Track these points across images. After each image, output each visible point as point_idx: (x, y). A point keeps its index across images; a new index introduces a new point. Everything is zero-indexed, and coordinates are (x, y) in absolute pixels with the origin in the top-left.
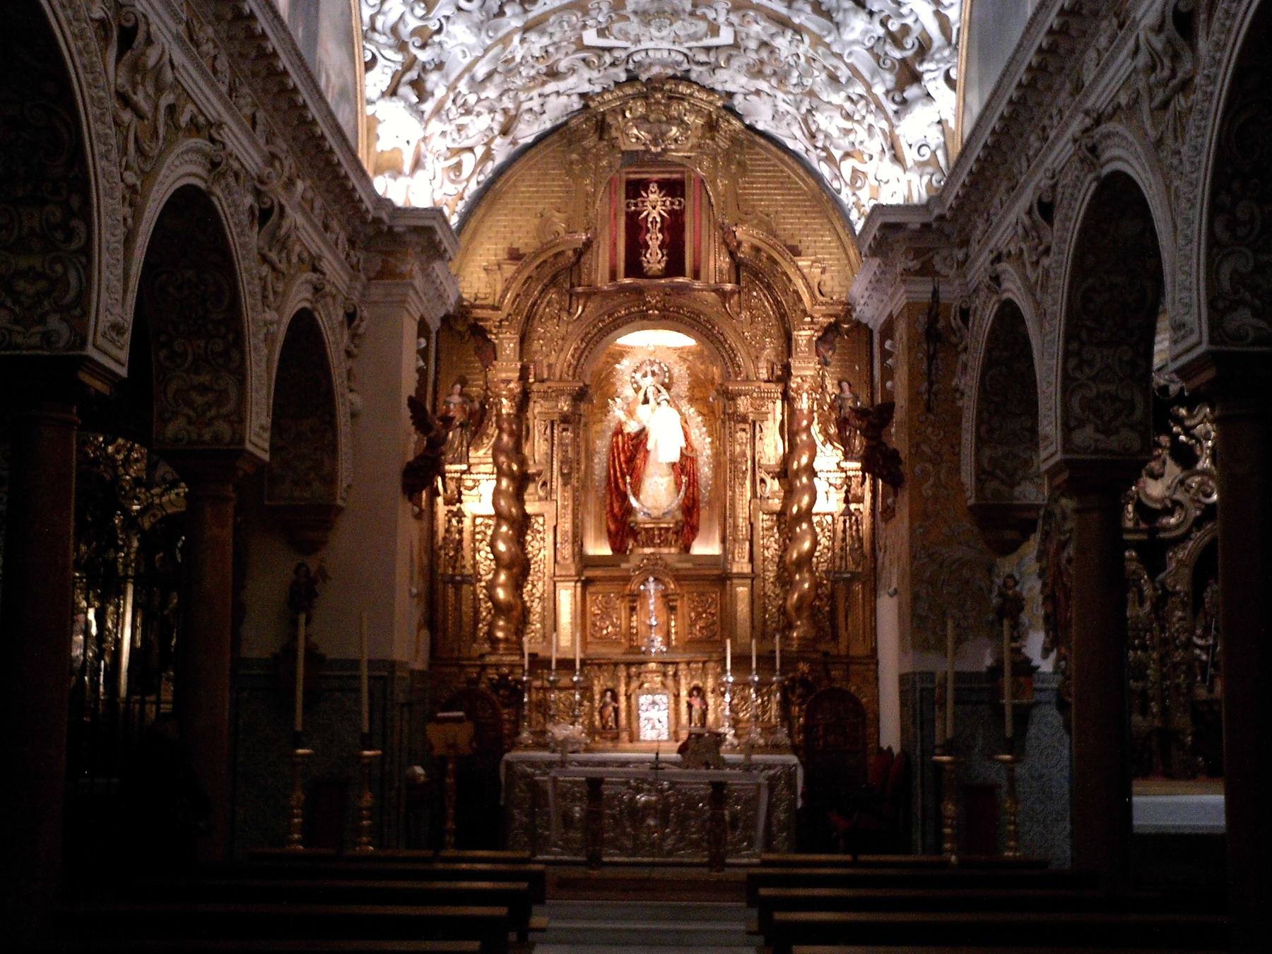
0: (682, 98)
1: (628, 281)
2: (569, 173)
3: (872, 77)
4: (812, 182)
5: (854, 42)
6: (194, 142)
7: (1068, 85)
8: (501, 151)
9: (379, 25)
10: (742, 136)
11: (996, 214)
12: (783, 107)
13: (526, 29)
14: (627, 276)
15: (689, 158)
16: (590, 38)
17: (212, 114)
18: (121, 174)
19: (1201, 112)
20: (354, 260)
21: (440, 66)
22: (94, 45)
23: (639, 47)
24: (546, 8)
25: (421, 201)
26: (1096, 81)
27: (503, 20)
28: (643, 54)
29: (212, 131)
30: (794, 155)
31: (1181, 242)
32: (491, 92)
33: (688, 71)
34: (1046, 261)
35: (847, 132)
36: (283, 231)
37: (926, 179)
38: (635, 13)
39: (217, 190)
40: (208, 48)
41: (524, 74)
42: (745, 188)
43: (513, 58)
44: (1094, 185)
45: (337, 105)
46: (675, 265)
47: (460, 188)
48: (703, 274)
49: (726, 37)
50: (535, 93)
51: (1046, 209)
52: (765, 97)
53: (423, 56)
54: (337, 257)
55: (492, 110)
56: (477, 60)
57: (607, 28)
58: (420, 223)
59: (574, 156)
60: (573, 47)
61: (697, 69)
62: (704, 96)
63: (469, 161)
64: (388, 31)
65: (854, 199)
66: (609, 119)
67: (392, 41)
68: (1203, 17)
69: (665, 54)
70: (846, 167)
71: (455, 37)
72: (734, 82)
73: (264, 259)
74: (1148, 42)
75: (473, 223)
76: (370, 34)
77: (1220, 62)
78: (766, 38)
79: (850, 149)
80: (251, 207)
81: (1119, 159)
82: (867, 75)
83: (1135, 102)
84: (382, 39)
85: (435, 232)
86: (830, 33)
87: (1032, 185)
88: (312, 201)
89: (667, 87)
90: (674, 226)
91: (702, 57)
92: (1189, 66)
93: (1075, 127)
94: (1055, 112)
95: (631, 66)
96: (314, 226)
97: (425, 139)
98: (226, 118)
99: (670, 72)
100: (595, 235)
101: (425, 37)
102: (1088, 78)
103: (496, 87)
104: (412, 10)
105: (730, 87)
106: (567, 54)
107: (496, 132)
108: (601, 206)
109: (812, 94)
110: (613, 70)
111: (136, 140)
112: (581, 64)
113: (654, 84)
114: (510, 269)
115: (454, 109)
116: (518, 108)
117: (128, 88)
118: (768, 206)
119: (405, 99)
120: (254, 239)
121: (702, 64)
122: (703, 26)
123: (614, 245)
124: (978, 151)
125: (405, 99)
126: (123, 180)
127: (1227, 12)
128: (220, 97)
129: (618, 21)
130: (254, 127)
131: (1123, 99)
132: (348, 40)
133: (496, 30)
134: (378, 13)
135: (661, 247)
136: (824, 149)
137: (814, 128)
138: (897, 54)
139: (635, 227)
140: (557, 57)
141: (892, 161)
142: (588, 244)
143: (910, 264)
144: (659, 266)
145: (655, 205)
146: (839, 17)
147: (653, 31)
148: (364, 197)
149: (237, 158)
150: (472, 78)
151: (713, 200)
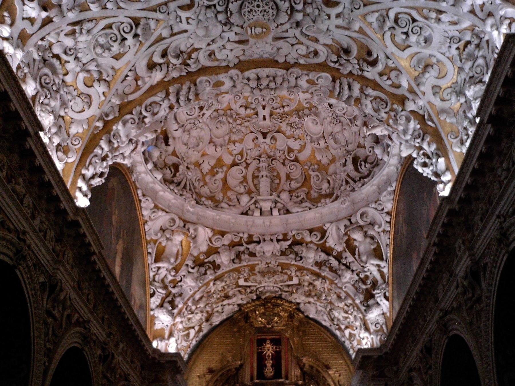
0: (279, 305)
1: (258, 381)
2: (233, 336)
3: (355, 296)
4: (333, 338)
5: (347, 282)
6: (76, 329)
7: (433, 299)
8: (206, 327)
9: (156, 279)
10: (304, 320)
11: (408, 352)
12: (320, 308)
13: (216, 280)
14: (257, 379)
15: (282, 329)
16: (241, 282)
17: (85, 317)
18: (45, 344)
19: (486, 311)
20: (143, 375)
21: (180, 295)
22: (39, 293)
23: (261, 286)
24: (224, 271)
25: (172, 350)
26: (443, 297)
27: (206, 276)
28: (263, 288)
29: (86, 324)
30: (326, 328)
31: (485, 365)
32: (202, 305)
33: (281, 294)
34: (430, 372)
35: (346, 318)
36: (113, 365)
37: (379, 337)
38: (259, 272)
39: (86, 349)
40: (85, 291)
41: (215, 297)
42: (305, 341)
43: (210, 291)
44: (447, 340)
45: (138, 312)
46: (278, 374)
47: (189, 343)
48: (289, 377)
49: (295, 281)
50: (219, 305)
51: (428, 350)
52: (312, 305)
53: (174, 291)
54: (136, 374)
55: (202, 312)
56: (196, 292)
57: (248, 278)
58: (170, 359)
59: (236, 330)
60: (235, 286)
61: (284, 294)
62: (288, 304)
63: (192, 332)
64: (160, 281)
65: (350, 345)
66: (250, 314)
67: (161, 285)
68: (482, 273)
69: (272, 288)
70: (347, 332)
71: (187, 283)
72: (299, 299)
73: (105, 377)
74: (461, 282)
75: (194, 357)
76: (153, 282)
77: (491, 291)
78: (311, 281)
79: (347, 325)
80: (100, 355)
81: (456, 329)
82: (352, 295)
83: (460, 307)
84: (157, 284)
85: (177, 363)
86: (336, 279)
87: (422, 340)
88: (126, 351)
89: (273, 301)
90: (277, 357)
91: (286, 289)
92: (479, 292)
93: (437, 316)
94: (428, 310)
95: (258, 293)
96: (127, 362)
97: (174, 324)
98: (92, 319)
99: (274, 295)
100: (244, 362)
101: (175, 284)
102: (440, 297)
103: (204, 302)
104: (170, 273)
105: (298, 301)
106: (232, 289)
107: (204, 320)
108: (247, 349)
109: (331, 303)
110: (251, 295)
111: (53, 330)
112: (238, 293)
113: (268, 300)
114: (209, 377)
115: (186, 312)
116: (212, 310)
117: (51, 309)
118: (316, 348)
119: (166, 308)
120: (100, 368)
121: (287, 292)
122: (286, 277)
123: (252, 367)
124: (399, 326)
125: (166, 308)
126: (45, 346)
127: (491, 271)
128: (89, 310)
129: (252, 275)
130: (103, 322)
131: (455, 305)
132: (144, 285)
133: (203, 280)
134: (156, 274)
135: (272, 366)
136: (337, 325)
137: (333, 317)
138: (364, 287)
139: (261, 359)
140: (228, 290)
141: (365, 330)
142: (241, 366)
143: (375, 373)
144: (272, 374)
145: (269, 349)
146: (340, 273)
147: (266, 279)
148: (148, 349)
149: (95, 335)
150: (194, 300)
151: (293, 347)
